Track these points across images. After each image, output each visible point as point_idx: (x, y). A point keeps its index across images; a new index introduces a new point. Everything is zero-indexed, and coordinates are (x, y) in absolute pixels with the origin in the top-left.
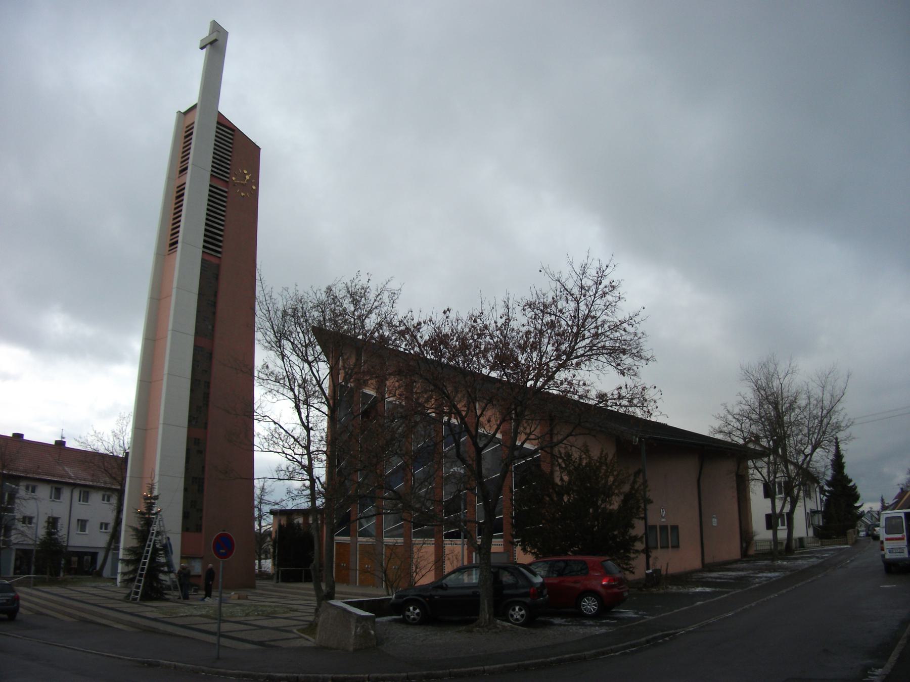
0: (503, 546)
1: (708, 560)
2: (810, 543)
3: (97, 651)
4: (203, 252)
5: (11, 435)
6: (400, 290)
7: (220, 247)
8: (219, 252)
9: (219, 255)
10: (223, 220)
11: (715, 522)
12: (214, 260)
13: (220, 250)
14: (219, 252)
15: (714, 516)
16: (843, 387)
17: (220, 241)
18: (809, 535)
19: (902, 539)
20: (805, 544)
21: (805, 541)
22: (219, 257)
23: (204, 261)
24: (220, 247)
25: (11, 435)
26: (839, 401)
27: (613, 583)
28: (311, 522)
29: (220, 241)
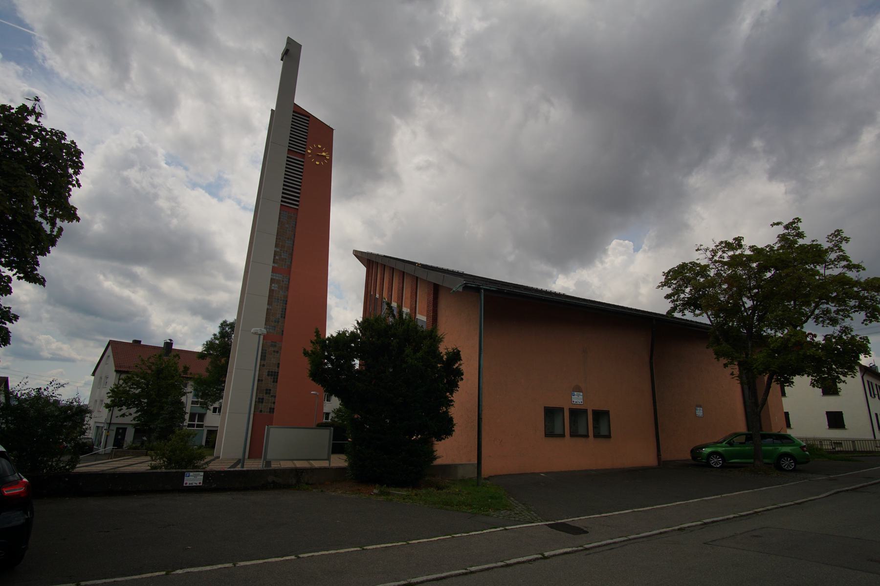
1: (665, 456)
4: (281, 205)
5: (131, 342)
18: (876, 438)
25: (131, 342)
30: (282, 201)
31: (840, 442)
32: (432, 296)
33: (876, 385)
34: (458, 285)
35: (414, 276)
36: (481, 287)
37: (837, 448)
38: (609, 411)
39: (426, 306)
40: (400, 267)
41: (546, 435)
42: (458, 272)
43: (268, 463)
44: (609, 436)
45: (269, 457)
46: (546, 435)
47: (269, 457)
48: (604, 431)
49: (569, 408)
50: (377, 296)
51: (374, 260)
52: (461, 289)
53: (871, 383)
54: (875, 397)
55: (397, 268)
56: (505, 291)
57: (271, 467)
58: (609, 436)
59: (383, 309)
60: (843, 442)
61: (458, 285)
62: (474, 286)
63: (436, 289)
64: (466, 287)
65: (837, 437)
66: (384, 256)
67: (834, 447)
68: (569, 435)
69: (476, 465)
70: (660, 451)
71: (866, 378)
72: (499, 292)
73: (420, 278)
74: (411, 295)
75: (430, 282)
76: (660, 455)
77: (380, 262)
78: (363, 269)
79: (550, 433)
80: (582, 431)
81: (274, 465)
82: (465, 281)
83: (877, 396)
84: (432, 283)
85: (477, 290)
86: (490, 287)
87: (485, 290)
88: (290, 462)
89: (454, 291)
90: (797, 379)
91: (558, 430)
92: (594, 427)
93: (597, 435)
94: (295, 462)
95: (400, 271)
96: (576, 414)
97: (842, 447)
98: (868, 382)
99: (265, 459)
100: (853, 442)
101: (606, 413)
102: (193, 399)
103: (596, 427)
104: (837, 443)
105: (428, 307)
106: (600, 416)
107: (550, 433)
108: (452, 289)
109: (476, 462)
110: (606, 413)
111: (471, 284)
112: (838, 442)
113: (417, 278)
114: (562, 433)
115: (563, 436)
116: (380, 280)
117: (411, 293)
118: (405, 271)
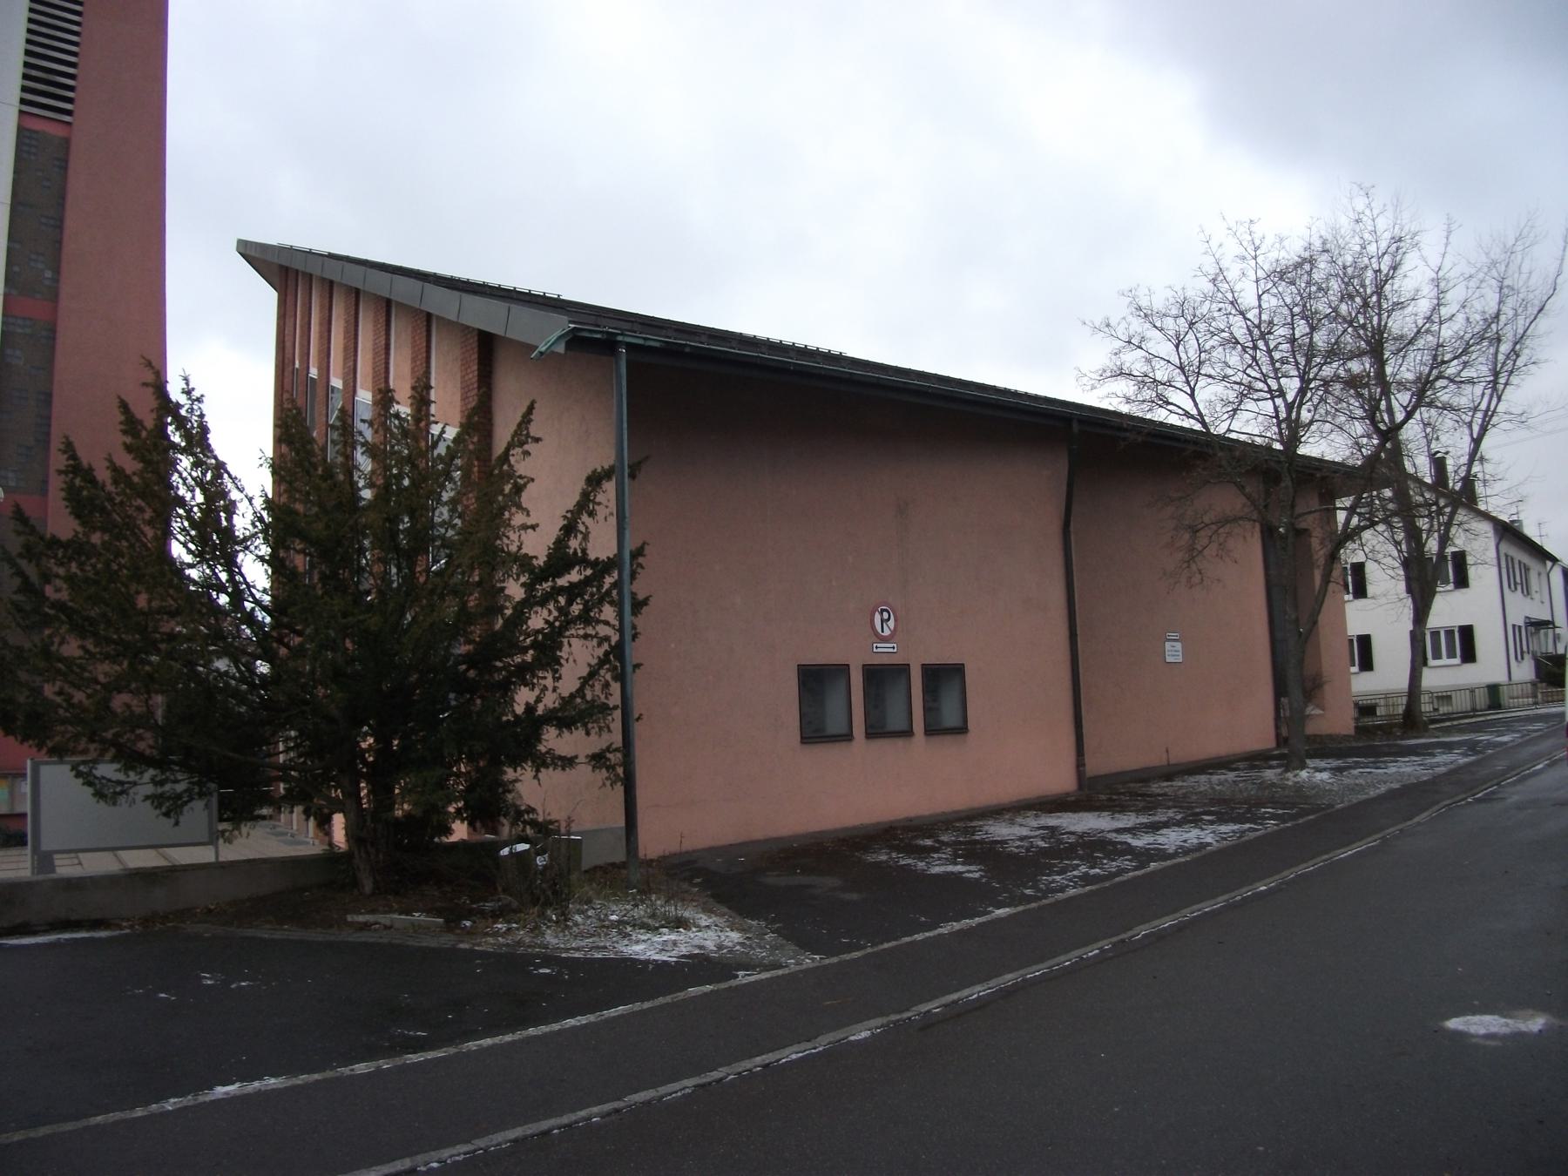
0: (1164, 763)
1: (1095, 766)
2: (1518, 698)
3: (802, 1052)
4: (21, 112)
6: (1233, 261)
7: (70, 100)
8: (69, 113)
9: (67, 118)
10: (74, 54)
11: (1174, 652)
12: (56, 131)
13: (68, 106)
14: (69, 113)
15: (1173, 635)
16: (1553, 270)
17: (71, 89)
18: (1513, 678)
19: (1168, 651)
20: (1505, 699)
21: (1505, 694)
22: (68, 123)
23: (22, 132)
24: (70, 100)
26: (1540, 310)
27: (884, 858)
28: (409, 725)
29: (71, 89)
30: (23, 101)
31: (1449, 693)
32: (476, 367)
33: (1520, 562)
34: (549, 334)
35: (422, 311)
36: (620, 338)
37: (1441, 709)
38: (963, 665)
39: (458, 397)
40: (381, 285)
41: (806, 739)
42: (544, 297)
43: (44, 861)
44: (962, 730)
45: (46, 846)
46: (806, 739)
47: (46, 846)
48: (950, 718)
49: (864, 665)
50: (314, 373)
51: (301, 268)
52: (561, 348)
53: (1512, 559)
54: (1516, 589)
55: (366, 289)
56: (687, 350)
57: (53, 871)
58: (962, 730)
59: (333, 412)
60: (1453, 694)
61: (549, 334)
62: (599, 336)
63: (486, 347)
64: (575, 341)
65: (1442, 684)
66: (331, 256)
67: (1436, 707)
68: (864, 734)
69: (623, 833)
70: (1083, 755)
71: (1504, 547)
72: (670, 351)
73: (438, 318)
74: (413, 369)
75: (468, 327)
76: (1084, 765)
77: (317, 272)
78: (268, 297)
79: (814, 733)
80: (895, 721)
81: (65, 868)
82: (570, 322)
83: (1519, 587)
84: (474, 329)
85: (608, 346)
86: (645, 339)
87: (629, 346)
88: (108, 856)
89: (541, 353)
90: (270, 584)
91: (835, 725)
92: (927, 710)
93: (932, 730)
94: (123, 854)
95: (377, 298)
96: (880, 677)
97: (1452, 705)
98: (1507, 556)
99: (36, 850)
100: (1472, 691)
101: (958, 670)
102: (1321, 505)
103: (930, 710)
104: (1443, 697)
105: (463, 399)
106: (944, 677)
107: (814, 733)
108: (537, 347)
109: (622, 823)
110: (958, 670)
111: (590, 331)
112: (1444, 694)
113: (429, 316)
114: (844, 730)
115: (848, 737)
116: (321, 324)
117: (414, 360)
118: (392, 297)
